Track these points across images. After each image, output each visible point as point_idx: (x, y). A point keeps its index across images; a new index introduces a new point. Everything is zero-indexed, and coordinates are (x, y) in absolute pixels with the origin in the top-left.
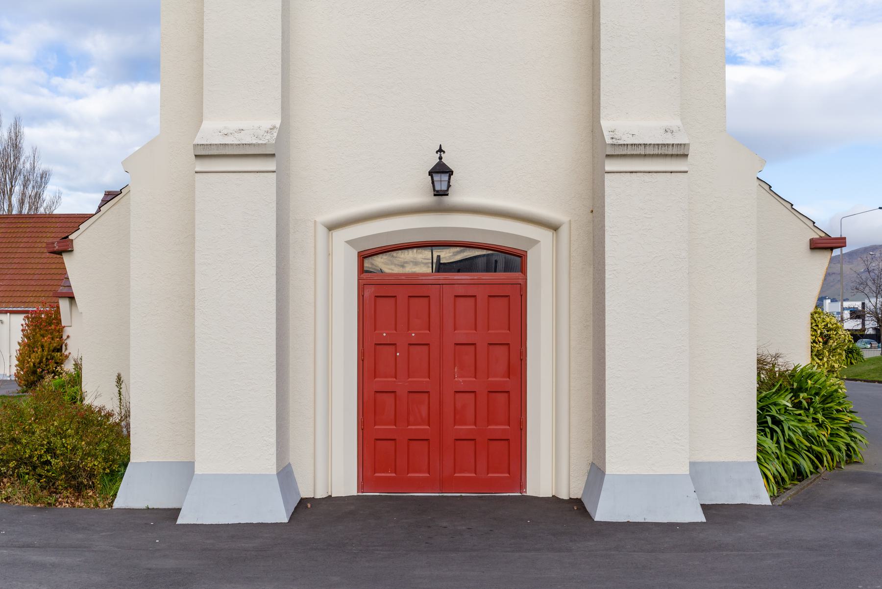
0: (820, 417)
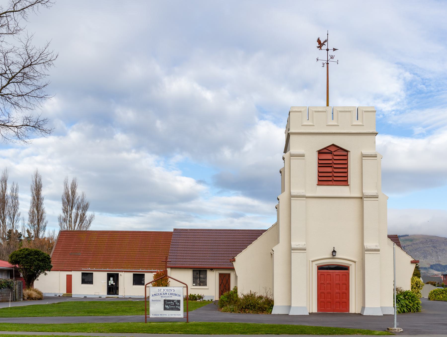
0: (410, 301)
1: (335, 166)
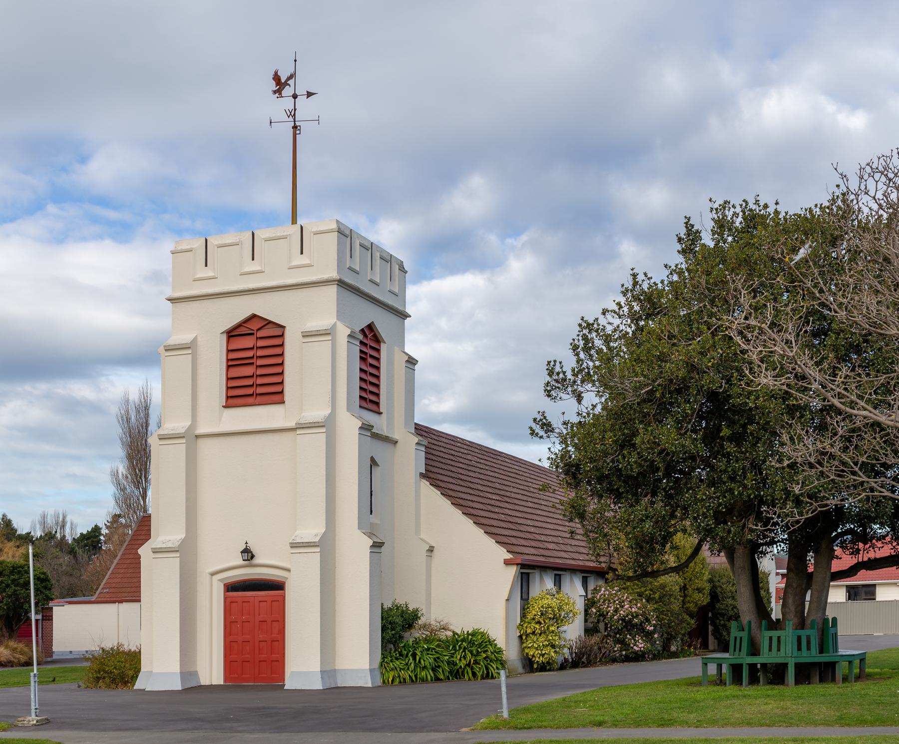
1: (260, 362)
